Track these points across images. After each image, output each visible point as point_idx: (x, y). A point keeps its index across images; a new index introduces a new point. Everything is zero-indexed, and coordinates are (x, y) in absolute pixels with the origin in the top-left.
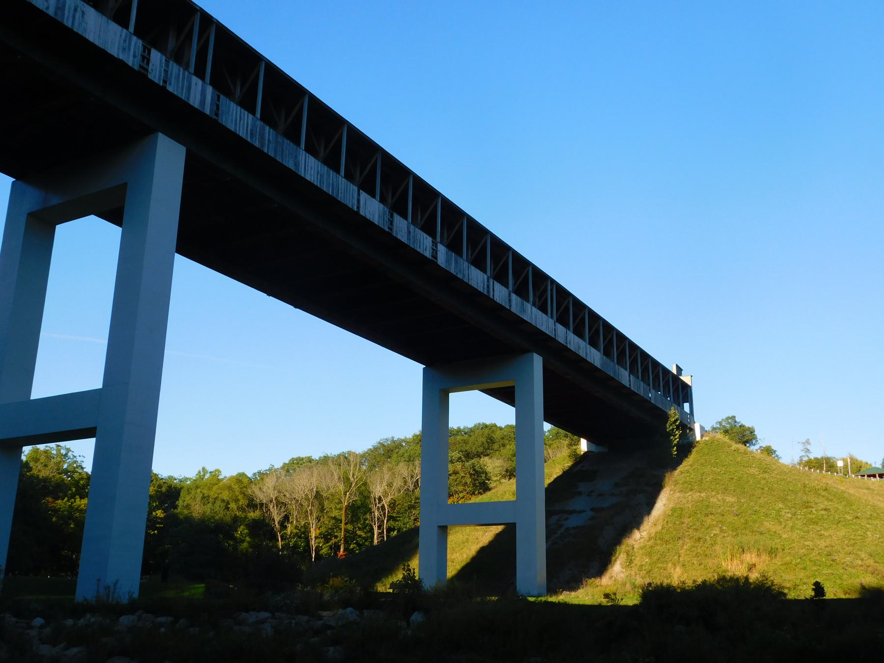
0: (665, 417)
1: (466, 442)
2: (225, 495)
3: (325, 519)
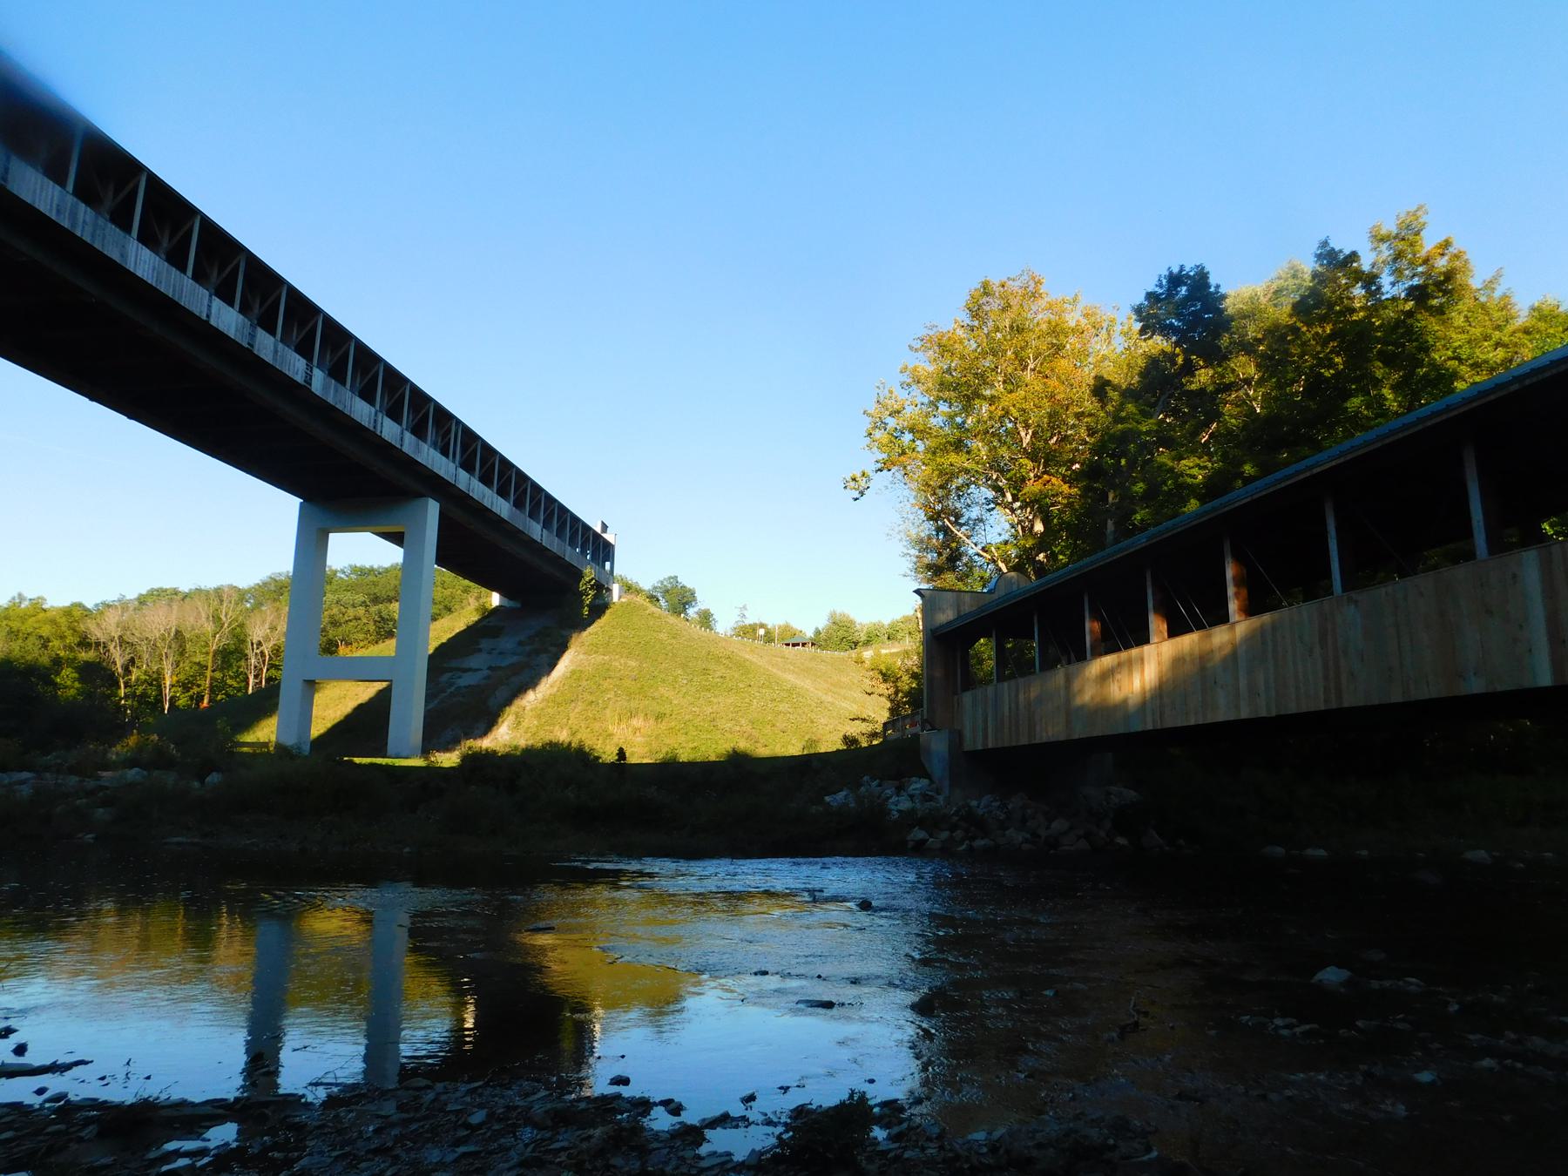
0: (579, 575)
1: (375, 584)
2: (46, 631)
3: (186, 665)
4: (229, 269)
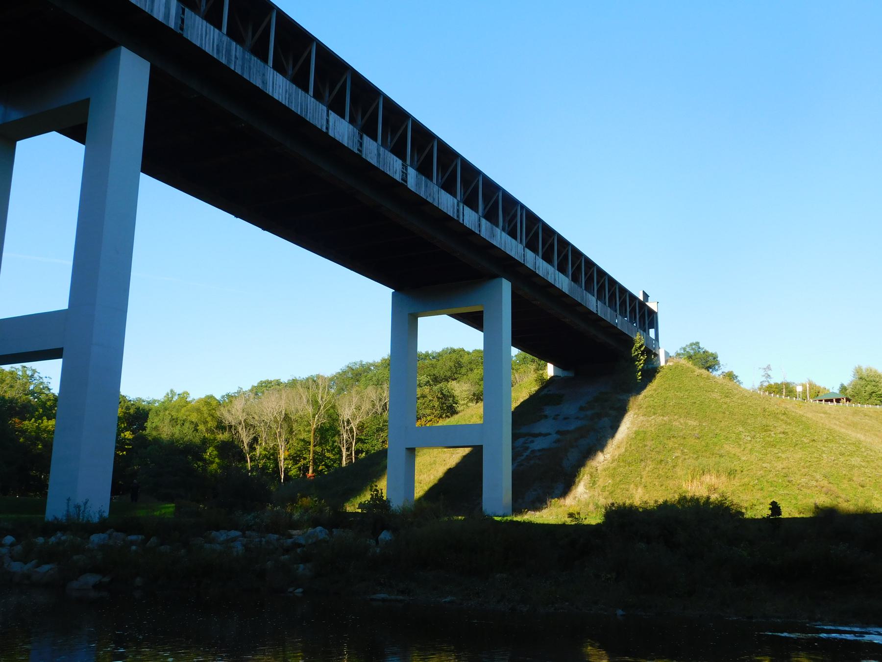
0: (630, 342)
1: (433, 366)
2: (194, 417)
3: (294, 442)
4: (338, 87)
